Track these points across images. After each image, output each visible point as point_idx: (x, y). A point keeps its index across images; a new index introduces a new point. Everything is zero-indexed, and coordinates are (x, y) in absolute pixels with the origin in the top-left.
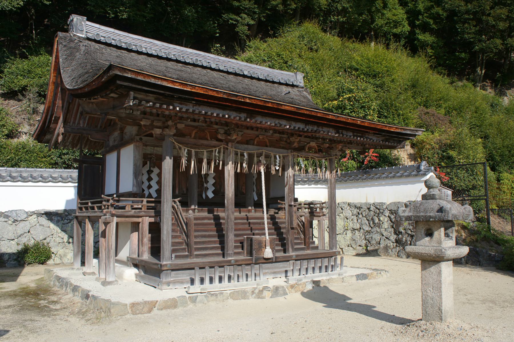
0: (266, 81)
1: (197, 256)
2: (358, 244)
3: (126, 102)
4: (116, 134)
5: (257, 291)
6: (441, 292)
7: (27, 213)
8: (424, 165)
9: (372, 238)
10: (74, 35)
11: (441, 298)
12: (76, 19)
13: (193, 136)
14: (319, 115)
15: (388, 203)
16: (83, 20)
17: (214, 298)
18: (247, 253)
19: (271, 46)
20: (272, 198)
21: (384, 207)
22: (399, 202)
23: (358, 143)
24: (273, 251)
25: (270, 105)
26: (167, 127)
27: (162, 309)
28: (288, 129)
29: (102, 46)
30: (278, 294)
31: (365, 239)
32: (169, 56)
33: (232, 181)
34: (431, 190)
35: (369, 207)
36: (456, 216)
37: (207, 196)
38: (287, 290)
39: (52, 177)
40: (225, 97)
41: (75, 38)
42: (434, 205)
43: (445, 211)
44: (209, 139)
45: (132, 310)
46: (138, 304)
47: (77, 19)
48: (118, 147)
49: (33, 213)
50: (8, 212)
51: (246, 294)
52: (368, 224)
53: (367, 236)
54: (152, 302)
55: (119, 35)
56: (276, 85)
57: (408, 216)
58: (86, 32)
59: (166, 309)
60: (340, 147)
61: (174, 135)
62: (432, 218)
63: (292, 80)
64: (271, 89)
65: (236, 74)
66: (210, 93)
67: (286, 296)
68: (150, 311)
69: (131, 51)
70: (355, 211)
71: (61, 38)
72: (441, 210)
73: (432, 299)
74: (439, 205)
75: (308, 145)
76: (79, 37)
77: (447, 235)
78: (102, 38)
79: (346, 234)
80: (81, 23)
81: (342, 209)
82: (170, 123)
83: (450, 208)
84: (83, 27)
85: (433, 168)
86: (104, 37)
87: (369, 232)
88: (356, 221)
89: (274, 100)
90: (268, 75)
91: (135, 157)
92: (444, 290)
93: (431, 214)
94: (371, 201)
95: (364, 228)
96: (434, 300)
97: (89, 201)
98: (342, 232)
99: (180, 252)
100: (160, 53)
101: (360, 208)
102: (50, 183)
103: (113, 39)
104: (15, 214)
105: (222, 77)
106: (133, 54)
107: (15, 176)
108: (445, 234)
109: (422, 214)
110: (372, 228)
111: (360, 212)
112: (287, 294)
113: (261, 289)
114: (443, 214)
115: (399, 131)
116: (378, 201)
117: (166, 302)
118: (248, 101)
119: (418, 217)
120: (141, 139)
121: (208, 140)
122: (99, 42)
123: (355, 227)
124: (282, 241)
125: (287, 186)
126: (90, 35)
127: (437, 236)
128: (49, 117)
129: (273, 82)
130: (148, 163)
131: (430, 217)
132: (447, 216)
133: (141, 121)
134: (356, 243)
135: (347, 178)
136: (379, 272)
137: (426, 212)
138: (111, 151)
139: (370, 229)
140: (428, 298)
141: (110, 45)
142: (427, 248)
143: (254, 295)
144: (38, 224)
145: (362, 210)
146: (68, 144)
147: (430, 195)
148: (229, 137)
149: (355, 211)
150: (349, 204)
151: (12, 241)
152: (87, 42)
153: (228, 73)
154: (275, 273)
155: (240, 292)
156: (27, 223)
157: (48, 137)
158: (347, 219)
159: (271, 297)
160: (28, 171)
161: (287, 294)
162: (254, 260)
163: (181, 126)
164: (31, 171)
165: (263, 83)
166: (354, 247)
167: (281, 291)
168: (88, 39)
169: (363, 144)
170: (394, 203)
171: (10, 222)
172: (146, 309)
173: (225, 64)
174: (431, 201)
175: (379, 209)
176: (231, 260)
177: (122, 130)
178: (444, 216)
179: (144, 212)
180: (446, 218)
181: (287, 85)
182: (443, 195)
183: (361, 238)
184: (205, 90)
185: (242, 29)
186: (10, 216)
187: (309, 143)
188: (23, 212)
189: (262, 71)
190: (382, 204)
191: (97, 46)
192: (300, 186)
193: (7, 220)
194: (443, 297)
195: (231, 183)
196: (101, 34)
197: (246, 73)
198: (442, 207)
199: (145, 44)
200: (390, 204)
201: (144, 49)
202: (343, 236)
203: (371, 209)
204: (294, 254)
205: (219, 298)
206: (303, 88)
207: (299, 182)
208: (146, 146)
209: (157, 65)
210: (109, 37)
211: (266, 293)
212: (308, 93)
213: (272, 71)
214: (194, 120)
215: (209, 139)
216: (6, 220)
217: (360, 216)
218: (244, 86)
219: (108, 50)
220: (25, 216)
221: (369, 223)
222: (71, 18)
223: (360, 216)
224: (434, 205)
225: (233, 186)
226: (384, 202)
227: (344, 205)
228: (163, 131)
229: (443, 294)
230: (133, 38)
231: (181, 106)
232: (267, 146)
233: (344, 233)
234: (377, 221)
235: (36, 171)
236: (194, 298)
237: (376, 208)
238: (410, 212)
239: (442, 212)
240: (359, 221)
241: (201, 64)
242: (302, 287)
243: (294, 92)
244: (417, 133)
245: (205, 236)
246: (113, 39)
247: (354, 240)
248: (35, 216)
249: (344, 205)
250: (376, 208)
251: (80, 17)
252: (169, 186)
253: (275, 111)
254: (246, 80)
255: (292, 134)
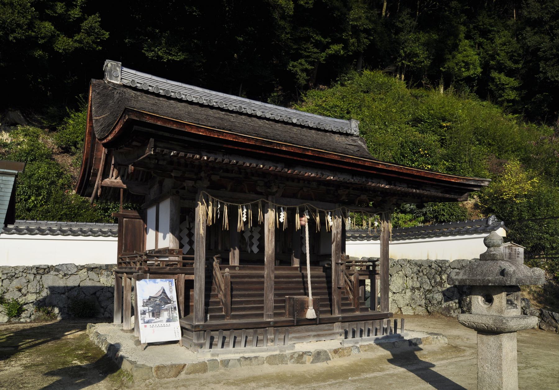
0: (317, 129)
1: (234, 317)
2: (418, 304)
3: (147, 151)
4: (156, 187)
5: (296, 356)
6: (501, 369)
7: (77, 267)
8: (492, 219)
9: (433, 297)
10: (109, 82)
11: (501, 378)
12: (109, 64)
13: (229, 188)
14: (367, 164)
15: (451, 261)
16: (118, 66)
17: (248, 362)
18: (289, 314)
19: (330, 95)
20: (322, 255)
21: (447, 265)
22: (463, 260)
23: (417, 196)
24: (316, 313)
25: (310, 153)
26: (201, 179)
27: (190, 373)
28: (197, 159)
29: (139, 93)
30: (319, 359)
31: (426, 299)
32: (211, 103)
33: (272, 237)
34: (492, 249)
35: (430, 264)
36: (521, 280)
37: (252, 251)
38: (330, 354)
39: (101, 231)
40: (258, 144)
41: (110, 85)
42: (495, 267)
43: (507, 274)
44: (247, 191)
45: (157, 374)
46: (164, 367)
47: (112, 64)
48: (156, 202)
49: (83, 267)
50: (58, 265)
51: (284, 358)
52: (429, 282)
53: (428, 296)
54: (179, 365)
55: (157, 82)
56: (328, 134)
57: (461, 279)
58: (122, 78)
59: (195, 373)
60: (394, 201)
61: (208, 188)
62: (492, 283)
63: (346, 129)
64: (322, 138)
65: (284, 122)
66: (240, 140)
67: (328, 361)
68: (176, 375)
69: (170, 98)
70: (415, 269)
71: (95, 85)
72: (503, 272)
73: (490, 377)
74: (500, 267)
75: (358, 198)
76: (114, 84)
77: (510, 303)
78: (139, 85)
79: (405, 293)
80: (115, 68)
81: (401, 266)
82: (202, 174)
83: (514, 271)
84: (118, 74)
85: (502, 223)
86: (141, 84)
87: (429, 291)
88: (415, 279)
89: (305, 146)
90: (319, 123)
91: (171, 211)
92: (505, 367)
93: (490, 278)
94: (433, 258)
95: (424, 287)
96: (492, 378)
97: (126, 257)
98: (401, 290)
99: (216, 312)
100: (201, 100)
101: (420, 266)
102: (91, 237)
103: (150, 86)
104: (65, 268)
105: (268, 126)
106: (172, 101)
107: (65, 230)
108: (508, 301)
109: (479, 277)
110: (433, 287)
111: (420, 270)
112: (330, 359)
113: (301, 353)
114: (504, 278)
115: (461, 181)
116: (440, 258)
117: (194, 365)
118: (284, 149)
119: (475, 280)
120: (178, 192)
121: (245, 192)
122: (135, 89)
123: (415, 286)
124: (325, 302)
125: (334, 244)
126: (125, 82)
127: (498, 304)
128: (87, 170)
129: (326, 131)
130: (187, 217)
131: (489, 281)
132: (510, 281)
133: (172, 172)
134: (415, 303)
135: (401, 234)
136: (436, 337)
137: (485, 275)
138: (150, 206)
139: (431, 288)
140: (485, 376)
141: (147, 92)
142: (484, 318)
143: (293, 360)
144: (88, 279)
145: (422, 267)
146: (109, 197)
147: (490, 255)
148: (269, 190)
149: (415, 269)
150: (409, 261)
151: (62, 295)
152: (122, 89)
153: (275, 121)
154: (319, 336)
155: (277, 357)
156: (77, 277)
157: (88, 190)
158: (407, 277)
159: (312, 362)
160: (78, 225)
161: (330, 359)
162: (295, 322)
163: (215, 178)
164: (81, 225)
165: (313, 131)
166: (414, 306)
167: (322, 356)
168: (125, 86)
169: (419, 196)
170: (458, 260)
171: (61, 276)
172: (173, 373)
173: (272, 112)
174: (490, 263)
175: (441, 267)
176: (270, 322)
177: (161, 183)
178: (506, 280)
179: (179, 269)
180: (508, 283)
181: (341, 134)
182: (514, 252)
183: (421, 297)
184: (234, 136)
185: (302, 78)
186: (61, 270)
187: (359, 196)
188: (73, 266)
189: (313, 119)
190: (445, 261)
191: (133, 93)
192: (351, 242)
193: (58, 273)
194: (504, 375)
195: (272, 239)
196: (137, 81)
197: (295, 121)
198: (504, 270)
199: (185, 91)
200: (454, 261)
201: (183, 96)
202: (402, 295)
203: (433, 267)
204: (340, 316)
205: (254, 362)
206: (358, 136)
207: (349, 237)
208: (184, 199)
209: (197, 113)
210: (145, 84)
211: (306, 358)
212: (363, 142)
213: (328, 121)
214: (227, 171)
215: (247, 191)
216: (57, 273)
217: (421, 274)
218: (291, 135)
219: (144, 97)
220: (76, 270)
221: (430, 282)
222: (106, 64)
223: (421, 274)
224: (495, 267)
225: (274, 243)
226: (446, 259)
227: (404, 262)
228: (195, 183)
229: (503, 372)
230: (172, 85)
231: (209, 155)
232: (312, 200)
233: (403, 292)
234: (438, 280)
235: (104, 227)
236: (226, 362)
237: (439, 266)
238: (465, 274)
239: (504, 276)
240: (419, 279)
241: (245, 112)
242: (347, 352)
243: (349, 140)
244: (482, 184)
245: (244, 296)
246: (150, 86)
247: (413, 299)
248: (85, 270)
249: (404, 262)
250: (439, 266)
251: (114, 63)
252: (202, 242)
253: (318, 161)
254: (295, 129)
255: (338, 185)
